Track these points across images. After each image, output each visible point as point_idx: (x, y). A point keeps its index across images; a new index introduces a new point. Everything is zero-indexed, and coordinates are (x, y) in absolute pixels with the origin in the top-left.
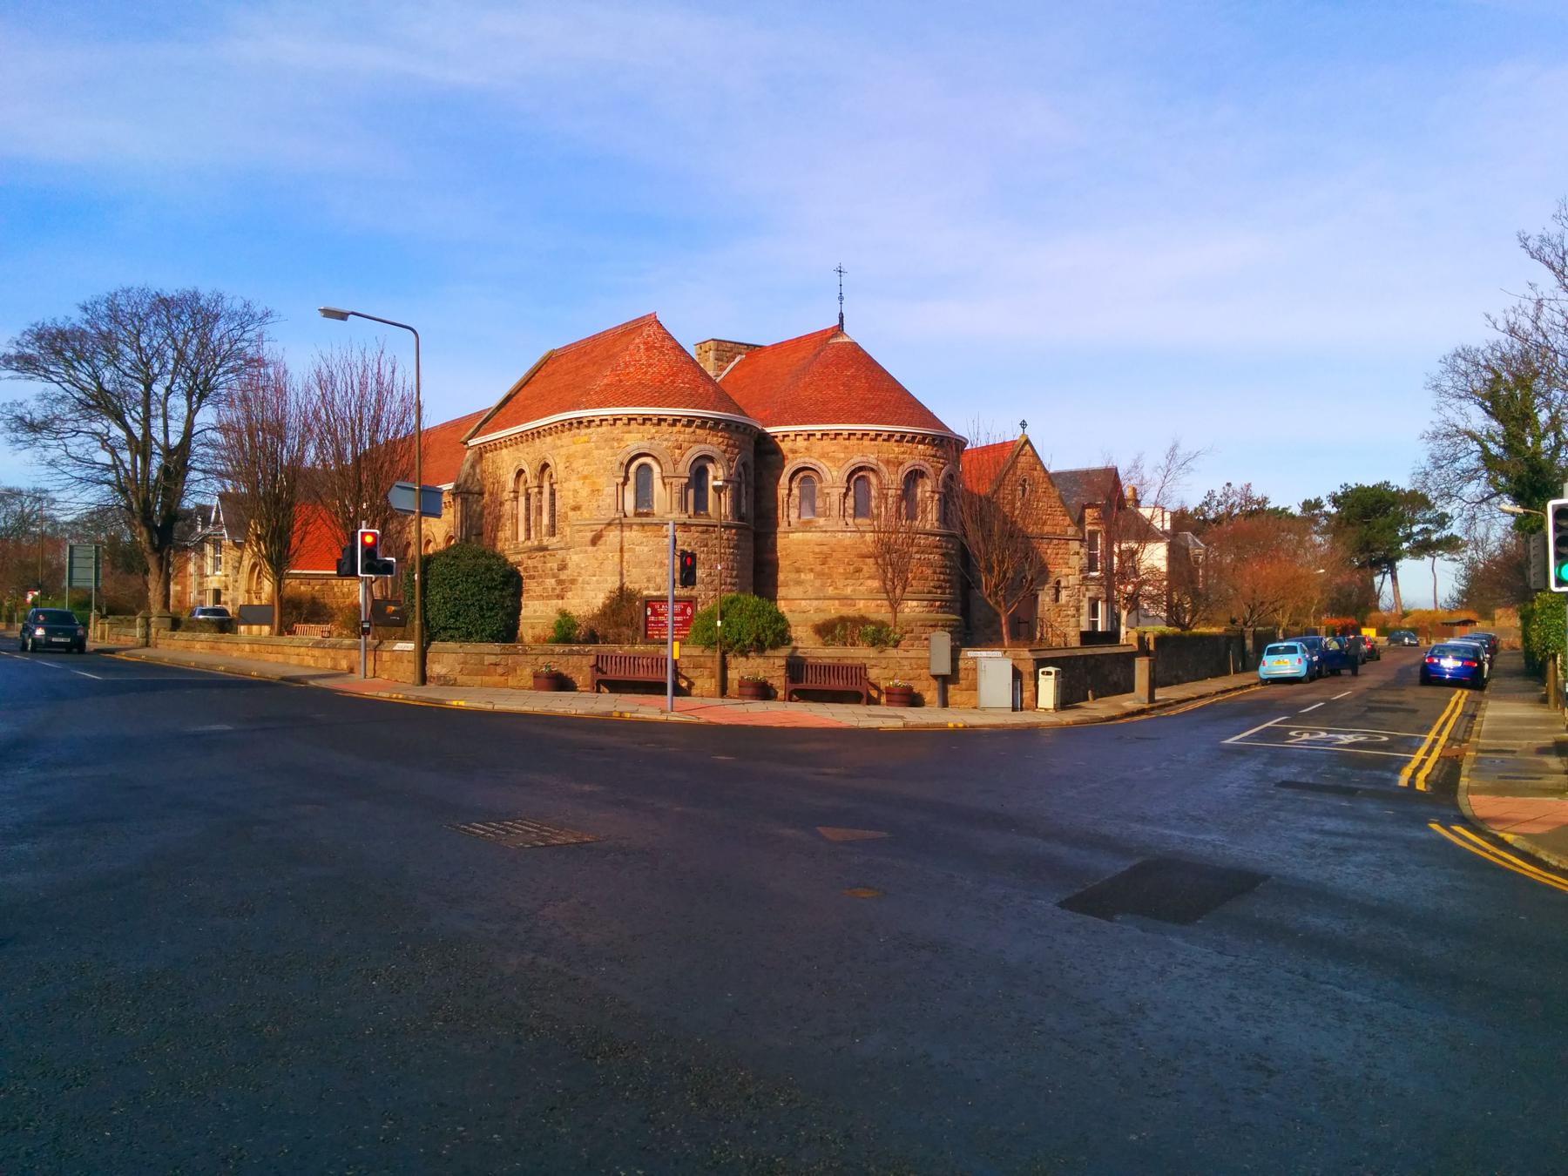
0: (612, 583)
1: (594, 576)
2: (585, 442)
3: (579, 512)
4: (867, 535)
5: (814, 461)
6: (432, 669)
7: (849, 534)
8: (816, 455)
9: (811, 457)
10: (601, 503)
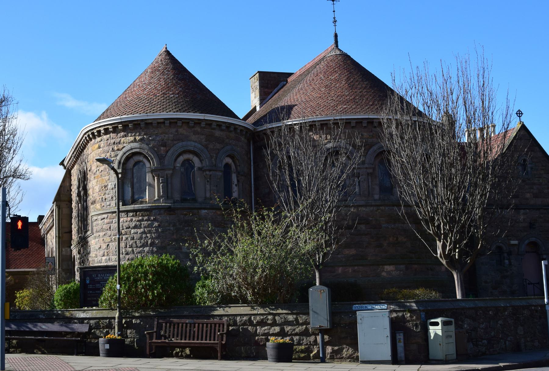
1: (104, 255)
10: (107, 196)
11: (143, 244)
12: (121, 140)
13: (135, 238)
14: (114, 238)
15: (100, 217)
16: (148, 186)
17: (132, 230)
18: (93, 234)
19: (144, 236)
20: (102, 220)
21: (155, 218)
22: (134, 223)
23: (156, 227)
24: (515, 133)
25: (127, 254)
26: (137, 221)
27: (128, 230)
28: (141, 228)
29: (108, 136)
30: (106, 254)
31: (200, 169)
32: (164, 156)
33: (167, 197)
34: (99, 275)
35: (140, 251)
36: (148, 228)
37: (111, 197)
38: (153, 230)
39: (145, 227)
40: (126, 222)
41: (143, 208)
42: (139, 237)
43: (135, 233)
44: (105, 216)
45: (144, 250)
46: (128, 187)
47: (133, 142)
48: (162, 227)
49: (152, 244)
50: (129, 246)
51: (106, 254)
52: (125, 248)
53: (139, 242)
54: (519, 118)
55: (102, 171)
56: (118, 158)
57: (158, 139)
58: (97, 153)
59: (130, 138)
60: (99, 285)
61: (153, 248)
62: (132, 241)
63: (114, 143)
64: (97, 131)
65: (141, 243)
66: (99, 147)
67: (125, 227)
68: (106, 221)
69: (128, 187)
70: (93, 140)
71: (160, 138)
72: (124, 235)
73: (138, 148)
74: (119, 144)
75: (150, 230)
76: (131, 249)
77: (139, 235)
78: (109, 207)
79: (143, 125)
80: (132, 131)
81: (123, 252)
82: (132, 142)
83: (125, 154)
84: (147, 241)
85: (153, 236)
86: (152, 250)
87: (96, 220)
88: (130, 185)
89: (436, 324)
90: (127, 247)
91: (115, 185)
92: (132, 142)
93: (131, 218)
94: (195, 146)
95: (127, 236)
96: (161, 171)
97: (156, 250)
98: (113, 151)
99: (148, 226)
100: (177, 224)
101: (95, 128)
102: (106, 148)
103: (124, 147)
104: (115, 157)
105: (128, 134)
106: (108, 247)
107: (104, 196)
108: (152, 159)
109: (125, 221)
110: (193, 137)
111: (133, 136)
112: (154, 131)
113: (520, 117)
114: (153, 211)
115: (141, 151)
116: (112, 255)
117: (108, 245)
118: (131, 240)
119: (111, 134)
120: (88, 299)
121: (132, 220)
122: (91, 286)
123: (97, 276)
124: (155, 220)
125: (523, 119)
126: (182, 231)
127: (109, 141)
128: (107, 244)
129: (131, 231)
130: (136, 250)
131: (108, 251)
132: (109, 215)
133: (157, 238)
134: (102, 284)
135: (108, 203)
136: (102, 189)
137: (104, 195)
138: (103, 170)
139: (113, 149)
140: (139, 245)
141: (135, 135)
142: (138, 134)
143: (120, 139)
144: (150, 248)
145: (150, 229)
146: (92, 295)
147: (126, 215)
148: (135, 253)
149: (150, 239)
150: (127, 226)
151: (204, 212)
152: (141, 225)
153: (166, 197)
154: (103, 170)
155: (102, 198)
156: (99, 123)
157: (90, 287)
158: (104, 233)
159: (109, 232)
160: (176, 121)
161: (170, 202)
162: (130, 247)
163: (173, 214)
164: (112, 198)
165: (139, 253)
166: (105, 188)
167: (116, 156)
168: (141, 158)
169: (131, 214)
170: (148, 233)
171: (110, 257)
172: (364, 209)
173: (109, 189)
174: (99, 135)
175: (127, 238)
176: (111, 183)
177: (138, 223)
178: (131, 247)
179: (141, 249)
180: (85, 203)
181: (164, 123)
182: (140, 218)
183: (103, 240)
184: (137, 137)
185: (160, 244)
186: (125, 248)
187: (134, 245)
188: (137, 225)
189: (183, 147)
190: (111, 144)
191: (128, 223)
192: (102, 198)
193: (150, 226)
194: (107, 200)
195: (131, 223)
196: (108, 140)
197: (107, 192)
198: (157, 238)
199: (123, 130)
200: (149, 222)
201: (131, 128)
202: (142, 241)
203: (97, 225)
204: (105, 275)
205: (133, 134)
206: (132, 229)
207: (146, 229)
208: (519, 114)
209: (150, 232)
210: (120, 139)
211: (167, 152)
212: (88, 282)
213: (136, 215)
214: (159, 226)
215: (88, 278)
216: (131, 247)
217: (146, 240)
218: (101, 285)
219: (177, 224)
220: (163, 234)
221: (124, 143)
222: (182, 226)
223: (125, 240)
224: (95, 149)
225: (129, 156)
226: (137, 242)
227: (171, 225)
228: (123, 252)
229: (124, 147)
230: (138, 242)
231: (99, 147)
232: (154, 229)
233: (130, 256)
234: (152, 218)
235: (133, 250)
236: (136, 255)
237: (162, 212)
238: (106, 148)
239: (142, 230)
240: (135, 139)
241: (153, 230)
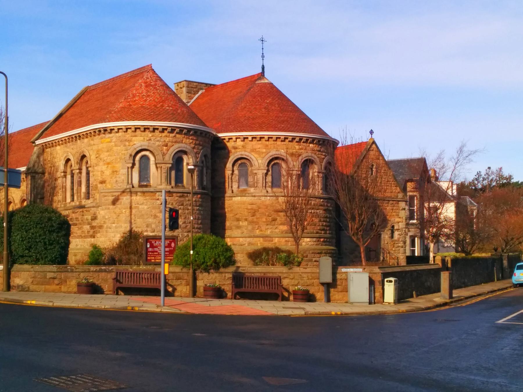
1: (114, 223)
7: (269, 198)
8: (249, 150)
9: (245, 151)
10: (118, 179)
24: (60, 119)
33: (128, 183)
34: (157, 242)
54: (371, 135)
59: (140, 138)
89: (391, 281)
113: (372, 134)
120: (416, 255)
122: (150, 249)
123: (155, 242)
125: (374, 136)
168: (243, 161)
208: (372, 132)
212: (148, 246)
215: (148, 244)
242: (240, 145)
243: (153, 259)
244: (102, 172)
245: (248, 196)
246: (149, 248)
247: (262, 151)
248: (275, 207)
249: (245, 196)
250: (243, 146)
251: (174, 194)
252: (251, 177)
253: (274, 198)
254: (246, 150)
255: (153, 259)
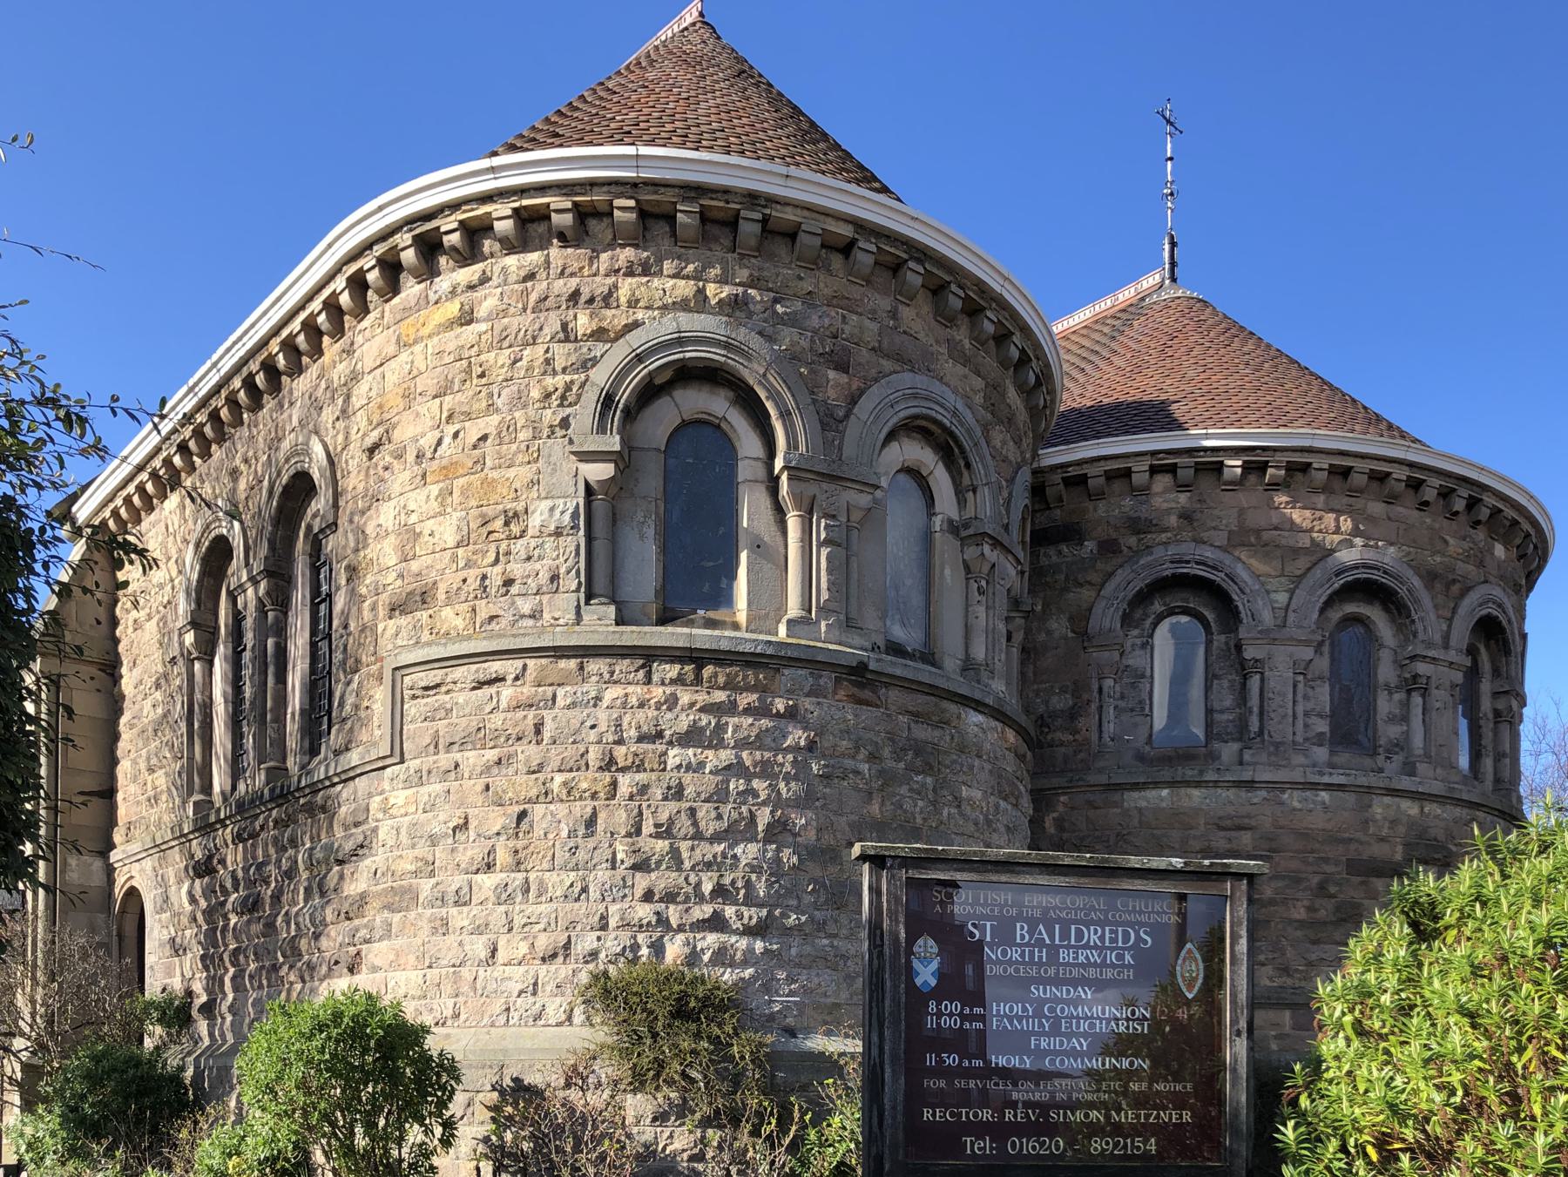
0: (428, 1020)
1: (489, 867)
2: (451, 324)
3: (423, 615)
4: (1376, 799)
5: (1209, 554)
6: (1246, 845)
7: (1325, 796)
8: (1221, 538)
9: (1199, 541)
10: (517, 569)
11: (733, 824)
12: (616, 286)
13: (689, 791)
14: (565, 784)
15: (462, 673)
16: (751, 551)
17: (671, 753)
18: (402, 762)
19: (737, 785)
20: (480, 685)
21: (795, 705)
22: (683, 716)
23: (796, 749)
25: (641, 866)
26: (702, 710)
27: (651, 746)
28: (719, 744)
29: (535, 257)
30: (503, 857)
31: (953, 528)
32: (841, 413)
35: (715, 856)
36: (759, 749)
37: (544, 577)
38: (782, 765)
39: (742, 744)
40: (641, 705)
41: (740, 649)
42: (711, 788)
43: (689, 768)
44: (510, 667)
45: (735, 856)
46: (642, 537)
47: (690, 311)
48: (824, 756)
49: (778, 831)
50: (657, 826)
51: (503, 857)
52: (629, 835)
53: (713, 814)
55: (484, 438)
56: (601, 376)
57: (814, 321)
58: (451, 346)
60: (1017, 1009)
61: (778, 850)
62: (673, 806)
63: (574, 296)
64: (461, 222)
65: (719, 817)
66: (467, 318)
67: (633, 733)
68: (507, 693)
69: (642, 537)
70: (411, 289)
71: (827, 321)
72: (623, 770)
73: (718, 343)
74: (607, 306)
75: (768, 760)
76: (662, 845)
77: (709, 782)
78: (531, 622)
79: (749, 229)
80: (680, 243)
81: (614, 854)
82: (683, 305)
83: (639, 358)
84: (752, 818)
85: (784, 791)
86: (778, 860)
87: (438, 686)
88: (650, 532)
90: (638, 832)
91: (575, 515)
92: (683, 305)
93: (669, 690)
94: (955, 413)
95: (641, 777)
96: (825, 486)
97: (795, 859)
98: (567, 340)
99: (757, 743)
100: (886, 752)
101: (454, 206)
102: (519, 322)
103: (636, 325)
104: (577, 371)
105: (660, 261)
106: (524, 826)
107: (498, 569)
108: (785, 415)
109: (633, 701)
110: (951, 369)
111: (687, 277)
112: (801, 278)
114: (786, 672)
115: (735, 363)
116: (546, 866)
117: (522, 815)
118: (665, 799)
119: (556, 253)
121: (672, 702)
124: (791, 714)
126: (904, 790)
127: (538, 289)
128: (517, 809)
129: (665, 753)
130: (692, 849)
131: (520, 844)
132: (531, 663)
133: (801, 803)
134: (1041, 1002)
135: (525, 606)
136: (484, 531)
137: (497, 561)
138: (492, 431)
139: (564, 326)
140: (710, 827)
141: (697, 276)
142: (715, 272)
143: (610, 281)
144: (765, 851)
145: (767, 755)
146: (959, 1084)
147: (641, 674)
148: (687, 865)
149: (764, 803)
150: (645, 728)
151: (975, 718)
152: (720, 728)
153: (842, 617)
154: (492, 431)
155: (484, 577)
156: (492, 169)
157: (946, 1022)
158: (492, 755)
159: (528, 752)
160: (905, 256)
161: (857, 641)
162: (658, 836)
163: (868, 704)
164: (554, 578)
165: (708, 866)
166: (507, 524)
167: (587, 364)
169: (672, 671)
170: (755, 775)
171: (532, 876)
172: (1439, 811)
173: (530, 532)
174: (469, 254)
175: (643, 789)
176: (549, 503)
177: (705, 719)
178: (665, 831)
179: (719, 848)
180: (270, 642)
181: (847, 249)
182: (720, 696)
183: (487, 788)
184: (711, 289)
185: (813, 832)
186: (629, 835)
187: (684, 825)
188: (702, 729)
189: (915, 396)
190: (550, 303)
191: (652, 713)
192: (484, 577)
193: (768, 741)
194: (514, 590)
195: (669, 715)
196: (531, 276)
197: (519, 547)
198: (801, 803)
199: (638, 236)
200: (765, 723)
201: (685, 225)
202: (726, 809)
203: (442, 713)
204: (1065, 935)
205: (691, 267)
206: (670, 743)
207: (745, 754)
209: (766, 770)
210: (610, 281)
211: (853, 400)
213: (698, 680)
214: (811, 746)
216: (665, 831)
217: (744, 809)
218: (1038, 1014)
219: (886, 752)
220: (827, 790)
221: (633, 303)
222: (902, 765)
223: (631, 798)
224: (425, 331)
225: (658, 381)
226: (700, 814)
227: (863, 753)
228: (620, 856)
229: (636, 325)
230: (704, 812)
231: (467, 318)
232: (790, 757)
233: (662, 880)
234: (780, 705)
235: (675, 853)
236: (693, 879)
237: (827, 679)
238: (519, 322)
239: (726, 756)
240: (701, 292)
241: (782, 765)
242: (1169, 511)
243: (980, 1129)
244: (411, 535)
245: (1216, 784)
246: (939, 993)
247: (1292, 543)
248: (1353, 847)
249: (1198, 784)
250: (1187, 516)
251: (894, 696)
252: (1226, 684)
253: (1350, 799)
254: (1205, 535)
255: (980, 1129)
